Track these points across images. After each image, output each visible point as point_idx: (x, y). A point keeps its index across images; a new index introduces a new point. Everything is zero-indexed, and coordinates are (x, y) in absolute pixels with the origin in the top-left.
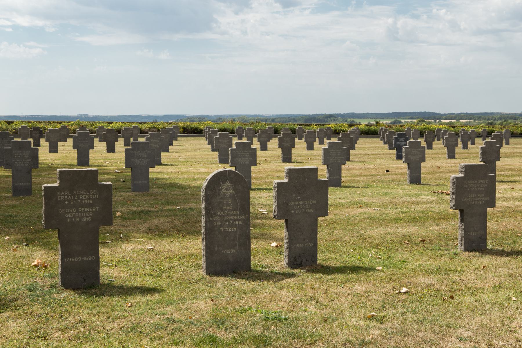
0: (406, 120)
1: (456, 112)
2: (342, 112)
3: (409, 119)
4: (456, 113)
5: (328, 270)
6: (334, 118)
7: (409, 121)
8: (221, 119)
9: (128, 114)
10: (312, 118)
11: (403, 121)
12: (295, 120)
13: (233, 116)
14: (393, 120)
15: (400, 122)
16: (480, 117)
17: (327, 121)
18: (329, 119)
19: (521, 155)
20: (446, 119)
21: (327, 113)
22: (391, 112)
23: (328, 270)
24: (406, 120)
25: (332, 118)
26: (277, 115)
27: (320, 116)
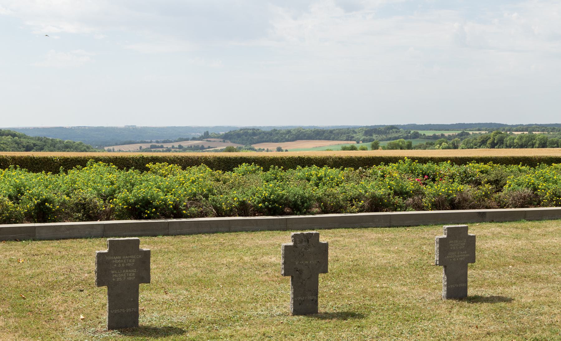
0: (474, 132)
1: (525, 122)
2: (402, 123)
3: (476, 130)
4: (524, 124)
5: (476, 299)
6: (396, 130)
7: (478, 132)
8: (276, 130)
9: (105, 125)
10: (372, 130)
11: (471, 133)
12: (14, 135)
13: (207, 128)
14: (460, 132)
15: (468, 134)
16: (554, 129)
17: (389, 133)
18: (391, 131)
19: (560, 234)
20: (517, 131)
21: (386, 124)
22: (455, 123)
23: (476, 299)
24: (474, 132)
25: (394, 130)
26: (336, 126)
27: (381, 128)
